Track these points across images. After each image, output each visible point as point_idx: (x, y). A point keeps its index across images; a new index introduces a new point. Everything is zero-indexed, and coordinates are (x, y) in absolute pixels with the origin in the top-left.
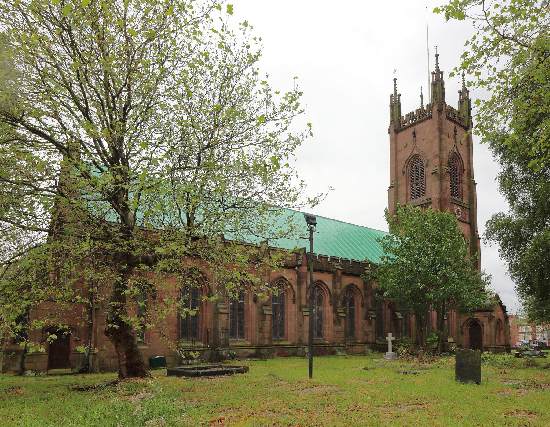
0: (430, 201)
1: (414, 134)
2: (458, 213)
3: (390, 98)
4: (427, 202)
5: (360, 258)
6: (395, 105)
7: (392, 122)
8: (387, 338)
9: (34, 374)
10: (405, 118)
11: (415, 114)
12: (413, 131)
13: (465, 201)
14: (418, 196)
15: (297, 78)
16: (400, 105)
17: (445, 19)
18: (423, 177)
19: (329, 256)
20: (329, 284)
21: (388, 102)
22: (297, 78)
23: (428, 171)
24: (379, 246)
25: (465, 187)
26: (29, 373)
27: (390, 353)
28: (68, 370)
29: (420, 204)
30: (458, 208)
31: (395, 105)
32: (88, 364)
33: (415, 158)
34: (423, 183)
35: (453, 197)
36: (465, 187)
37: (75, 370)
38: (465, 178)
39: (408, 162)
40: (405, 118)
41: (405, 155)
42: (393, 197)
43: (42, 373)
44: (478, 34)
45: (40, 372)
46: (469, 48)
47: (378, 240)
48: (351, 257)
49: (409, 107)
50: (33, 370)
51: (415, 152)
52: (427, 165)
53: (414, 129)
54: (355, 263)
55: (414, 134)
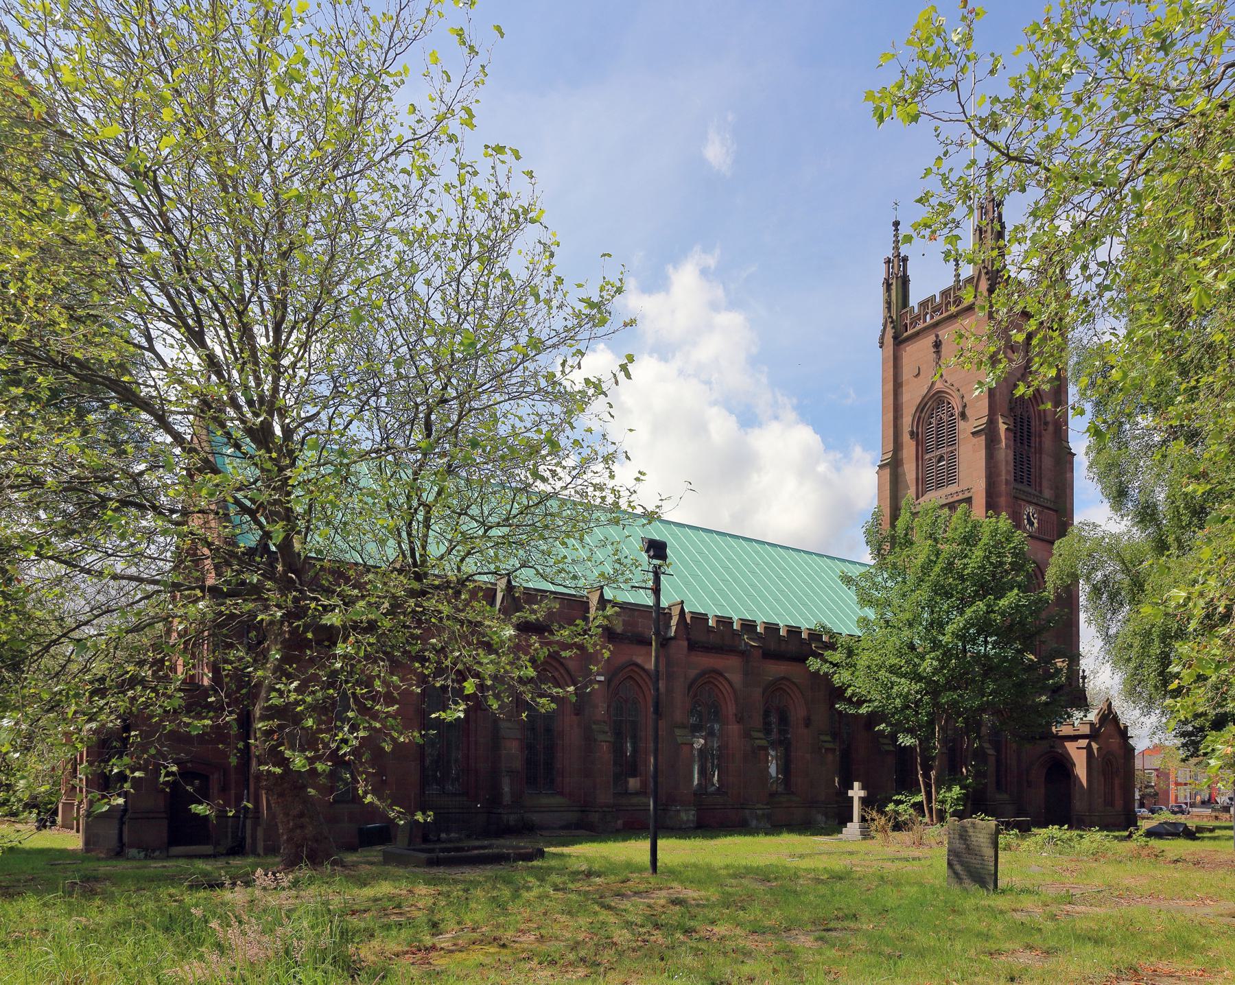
0: (967, 495)
1: (937, 345)
2: (1029, 519)
3: (884, 266)
4: (961, 497)
5: (806, 623)
7: (889, 320)
8: (850, 793)
9: (142, 854)
10: (916, 310)
11: (938, 299)
12: (932, 338)
13: (1047, 493)
14: (939, 485)
15: (610, 255)
16: (905, 281)
17: (875, 120)
18: (952, 442)
19: (735, 618)
20: (736, 678)
21: (881, 272)
22: (610, 255)
23: (965, 429)
24: (851, 595)
25: (1047, 462)
26: (133, 852)
27: (853, 828)
28: (208, 849)
29: (944, 502)
30: (1031, 509)
32: (244, 838)
33: (935, 401)
34: (952, 456)
35: (1020, 486)
36: (1047, 462)
37: (222, 849)
38: (1048, 442)
39: (921, 408)
40: (916, 310)
41: (912, 396)
42: (887, 486)
43: (157, 853)
44: (945, 154)
45: (153, 851)
46: (933, 184)
47: (848, 580)
48: (783, 620)
49: (929, 280)
50: (139, 847)
52: (963, 415)
54: (794, 632)
55: (937, 345)
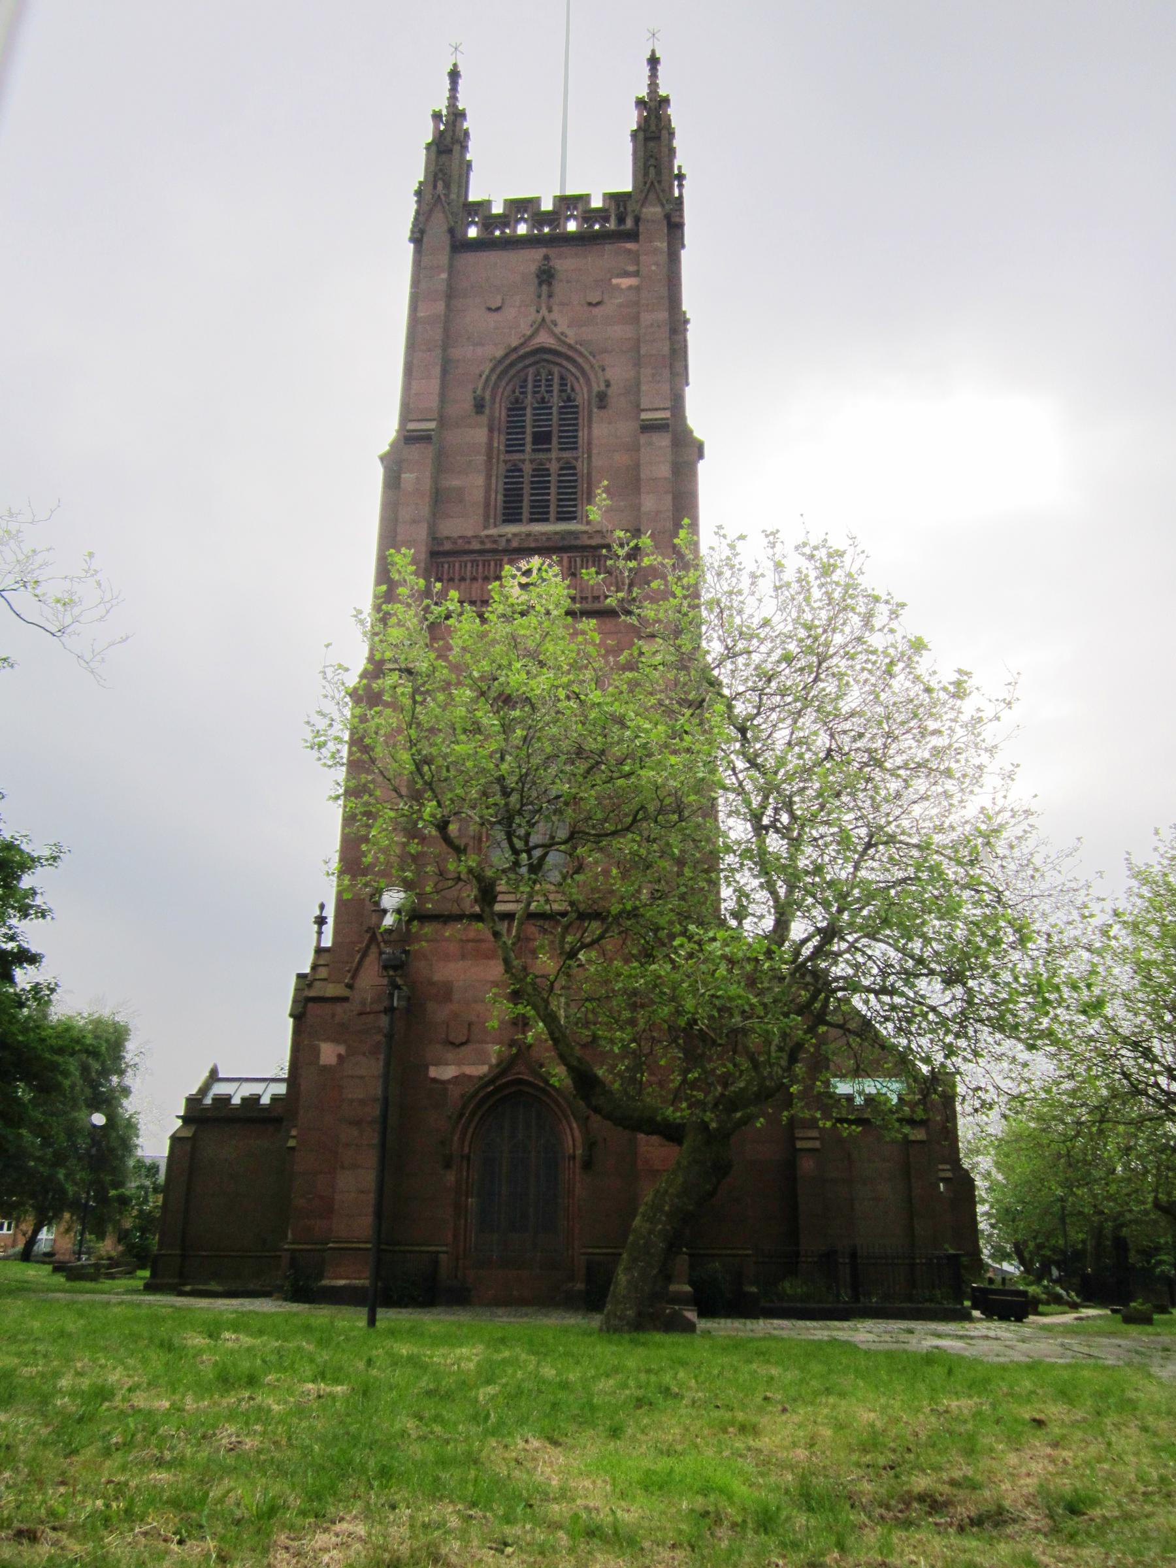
1: (546, 276)
6: (448, 146)
31: (448, 146)
51: (544, 339)
53: (546, 258)
55: (546, 276)
